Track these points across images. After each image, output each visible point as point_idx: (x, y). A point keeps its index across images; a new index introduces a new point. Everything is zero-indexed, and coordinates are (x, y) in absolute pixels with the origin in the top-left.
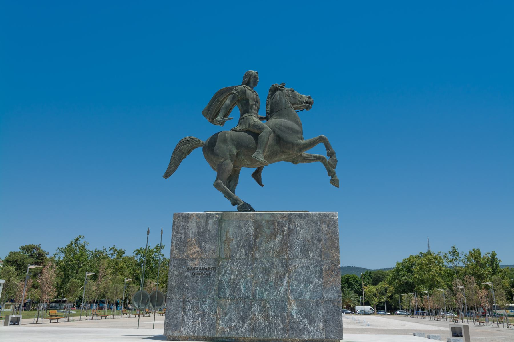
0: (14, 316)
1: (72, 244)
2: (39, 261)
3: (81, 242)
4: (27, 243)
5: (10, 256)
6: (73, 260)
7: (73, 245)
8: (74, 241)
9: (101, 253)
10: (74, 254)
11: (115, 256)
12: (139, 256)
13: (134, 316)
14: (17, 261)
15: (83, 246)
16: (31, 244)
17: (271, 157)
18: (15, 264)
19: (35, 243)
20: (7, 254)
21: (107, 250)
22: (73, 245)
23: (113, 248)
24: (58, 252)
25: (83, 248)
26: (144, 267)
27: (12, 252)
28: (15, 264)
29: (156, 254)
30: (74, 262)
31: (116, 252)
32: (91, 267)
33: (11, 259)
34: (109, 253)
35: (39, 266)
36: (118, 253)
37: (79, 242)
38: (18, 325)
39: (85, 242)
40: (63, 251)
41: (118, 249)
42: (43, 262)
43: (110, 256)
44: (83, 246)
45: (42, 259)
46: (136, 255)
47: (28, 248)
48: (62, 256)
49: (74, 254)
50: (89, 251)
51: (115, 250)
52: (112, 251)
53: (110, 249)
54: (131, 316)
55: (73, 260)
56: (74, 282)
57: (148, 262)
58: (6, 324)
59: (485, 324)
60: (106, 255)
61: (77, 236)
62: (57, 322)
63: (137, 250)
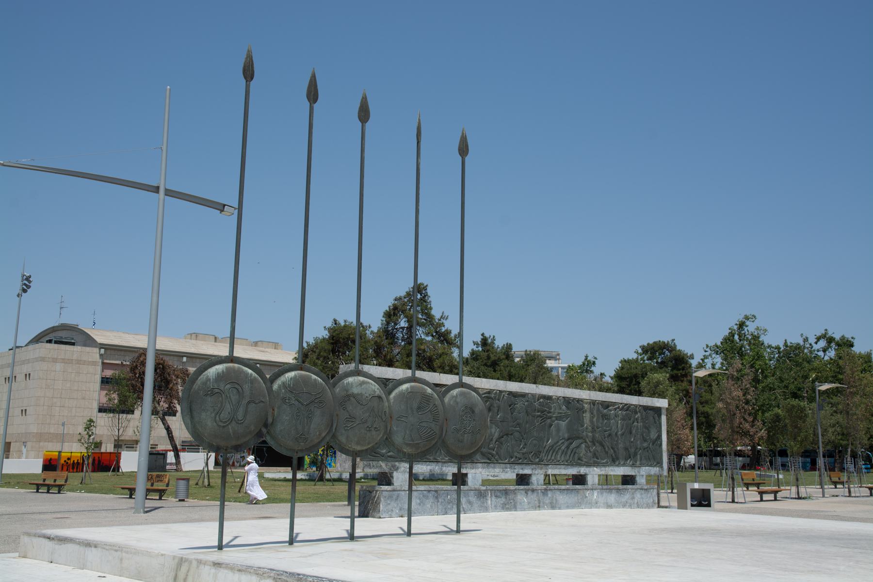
0: (696, 486)
2: (679, 373)
3: (751, 327)
5: (622, 368)
7: (736, 337)
8: (735, 327)
9: (798, 347)
10: (742, 355)
11: (832, 353)
15: (756, 338)
16: (657, 340)
17: (637, 358)
19: (666, 338)
20: (617, 365)
21: (812, 340)
22: (736, 337)
23: (823, 336)
24: (707, 354)
27: (625, 361)
31: (833, 345)
32: (781, 380)
34: (816, 347)
36: (838, 344)
37: (746, 329)
39: (757, 329)
40: (716, 350)
41: (837, 337)
42: (686, 375)
43: (821, 354)
44: (756, 338)
45: (683, 369)
47: (653, 348)
48: (718, 360)
49: (742, 355)
50: (770, 346)
51: (830, 340)
52: (822, 343)
53: (818, 339)
56: (793, 406)
58: (682, 506)
60: (811, 352)
62: (776, 499)
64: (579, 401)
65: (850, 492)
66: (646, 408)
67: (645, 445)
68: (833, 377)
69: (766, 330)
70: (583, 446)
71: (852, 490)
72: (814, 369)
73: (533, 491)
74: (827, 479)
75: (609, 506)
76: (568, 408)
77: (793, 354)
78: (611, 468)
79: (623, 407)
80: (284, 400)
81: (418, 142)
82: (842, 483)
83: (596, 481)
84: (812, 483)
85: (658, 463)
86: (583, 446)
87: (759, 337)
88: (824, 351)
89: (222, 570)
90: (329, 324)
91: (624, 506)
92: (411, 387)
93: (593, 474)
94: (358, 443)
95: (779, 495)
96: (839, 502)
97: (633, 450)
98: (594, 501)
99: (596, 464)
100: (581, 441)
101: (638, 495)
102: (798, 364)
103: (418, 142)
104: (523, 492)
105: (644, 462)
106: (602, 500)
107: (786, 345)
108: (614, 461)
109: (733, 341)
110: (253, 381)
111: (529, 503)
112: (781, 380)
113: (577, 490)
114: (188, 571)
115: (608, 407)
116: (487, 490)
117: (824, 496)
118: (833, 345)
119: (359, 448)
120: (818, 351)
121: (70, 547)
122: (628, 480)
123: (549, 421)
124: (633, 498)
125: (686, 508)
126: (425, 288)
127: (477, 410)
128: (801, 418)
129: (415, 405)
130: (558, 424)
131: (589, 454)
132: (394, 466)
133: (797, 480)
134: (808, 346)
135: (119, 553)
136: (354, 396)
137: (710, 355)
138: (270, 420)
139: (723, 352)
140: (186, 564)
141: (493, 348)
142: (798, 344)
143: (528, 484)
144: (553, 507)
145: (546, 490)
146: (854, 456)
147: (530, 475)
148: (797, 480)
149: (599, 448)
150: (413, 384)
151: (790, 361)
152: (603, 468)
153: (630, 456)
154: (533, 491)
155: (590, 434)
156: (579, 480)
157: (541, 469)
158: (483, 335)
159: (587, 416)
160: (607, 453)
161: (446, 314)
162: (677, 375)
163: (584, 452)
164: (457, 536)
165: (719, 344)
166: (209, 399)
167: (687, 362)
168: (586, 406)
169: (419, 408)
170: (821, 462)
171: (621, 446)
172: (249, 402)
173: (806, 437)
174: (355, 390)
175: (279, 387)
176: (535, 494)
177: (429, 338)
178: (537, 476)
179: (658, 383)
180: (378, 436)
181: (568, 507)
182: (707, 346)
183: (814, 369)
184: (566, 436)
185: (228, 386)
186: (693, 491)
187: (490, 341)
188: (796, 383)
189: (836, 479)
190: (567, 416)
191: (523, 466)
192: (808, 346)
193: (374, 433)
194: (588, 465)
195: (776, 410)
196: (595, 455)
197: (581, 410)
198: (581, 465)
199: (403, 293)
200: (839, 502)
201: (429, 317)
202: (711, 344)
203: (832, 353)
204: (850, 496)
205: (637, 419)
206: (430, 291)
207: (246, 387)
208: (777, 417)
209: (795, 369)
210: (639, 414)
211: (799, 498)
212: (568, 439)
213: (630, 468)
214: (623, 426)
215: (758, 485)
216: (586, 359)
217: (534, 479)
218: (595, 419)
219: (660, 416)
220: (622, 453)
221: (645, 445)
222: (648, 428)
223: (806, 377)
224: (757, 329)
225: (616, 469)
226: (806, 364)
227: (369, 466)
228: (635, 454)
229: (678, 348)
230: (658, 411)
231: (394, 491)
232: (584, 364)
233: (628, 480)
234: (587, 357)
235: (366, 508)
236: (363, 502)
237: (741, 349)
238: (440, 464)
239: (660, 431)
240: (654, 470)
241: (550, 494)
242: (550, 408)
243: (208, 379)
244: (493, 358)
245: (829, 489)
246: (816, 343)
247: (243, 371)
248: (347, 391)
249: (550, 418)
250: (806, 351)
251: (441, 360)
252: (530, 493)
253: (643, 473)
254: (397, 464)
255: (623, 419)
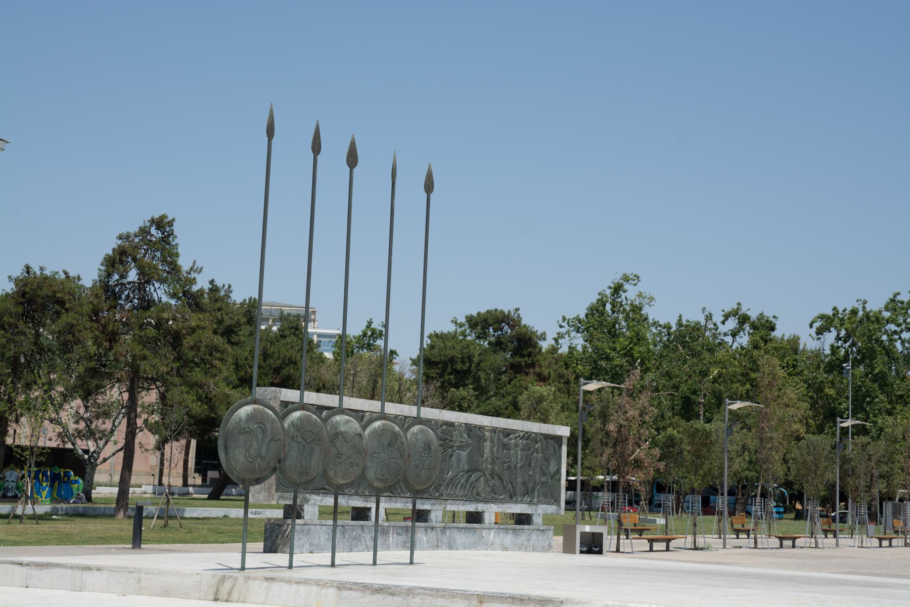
0: (588, 529)
1: (602, 302)
3: (630, 294)
4: (480, 306)
6: (613, 354)
7: (608, 307)
8: (608, 292)
9: (695, 330)
12: (830, 338)
13: (876, 542)
14: (452, 360)
15: (636, 309)
18: (449, 370)
19: (506, 306)
21: (718, 318)
22: (608, 307)
23: (734, 313)
24: (563, 330)
25: (636, 313)
26: (854, 373)
27: (437, 335)
28: (449, 370)
29: (892, 327)
30: (617, 361)
31: (747, 327)
33: (435, 356)
34: (722, 329)
35: (748, 404)
36: (754, 327)
37: (624, 295)
38: (600, 552)
39: (640, 295)
40: (578, 325)
41: (754, 315)
42: (533, 365)
43: (729, 339)
44: (636, 309)
45: (529, 355)
46: (820, 332)
47: (485, 321)
48: (579, 341)
50: (656, 324)
51: (744, 319)
52: (732, 324)
53: (727, 317)
54: (867, 542)
55: (613, 354)
56: (697, 430)
57: (866, 356)
58: (568, 548)
59: (894, 542)
60: (715, 336)
61: (618, 278)
62: (668, 550)
63: (822, 317)
64: (481, 428)
65: (756, 542)
66: (547, 437)
67: (544, 479)
68: (742, 375)
69: (652, 299)
70: (482, 479)
71: (759, 540)
72: (717, 363)
73: (432, 528)
74: (728, 526)
75: (505, 548)
76: (469, 437)
77: (688, 337)
78: (508, 505)
79: (524, 435)
80: (293, 438)
81: (393, 184)
82: (747, 532)
83: (493, 519)
84: (709, 532)
85: (556, 501)
86: (482, 479)
87: (640, 309)
88: (734, 334)
89: (276, 583)
90: (18, 271)
91: (520, 549)
92: (383, 425)
93: (491, 511)
94: (343, 478)
95: (673, 544)
96: (743, 554)
97: (530, 485)
98: (490, 542)
99: (494, 501)
100: (479, 474)
101: (534, 537)
102: (695, 354)
103: (393, 184)
104: (423, 530)
105: (542, 499)
106: (497, 541)
107: (680, 324)
108: (512, 497)
109: (602, 313)
110: (273, 421)
111: (428, 542)
112: (669, 375)
113: (475, 529)
114: (233, 586)
115: (508, 435)
116: (389, 526)
117: (724, 547)
118: (747, 327)
119: (342, 482)
120: (725, 334)
121: (57, 572)
122: (523, 520)
123: (450, 450)
124: (529, 540)
125: (574, 553)
126: (170, 224)
127: (433, 448)
128: (705, 445)
129: (386, 442)
130: (459, 454)
131: (488, 489)
132: (305, 498)
133: (695, 525)
134: (712, 326)
135: (135, 574)
136: (341, 433)
137: (568, 332)
138: (282, 456)
139: (587, 329)
140: (230, 580)
141: (227, 304)
142: (698, 323)
143: (426, 521)
144: (450, 547)
145: (444, 528)
146: (764, 495)
147: (429, 511)
148: (695, 525)
149: (497, 482)
150: (383, 421)
151: (684, 348)
152: (500, 505)
153: (528, 492)
154: (432, 528)
155: (489, 466)
156: (475, 518)
157: (440, 504)
158: (212, 282)
159: (487, 445)
160: (505, 487)
161: (199, 264)
162: (519, 364)
163: (483, 486)
164: (411, 566)
165: (582, 316)
166: (242, 437)
167: (535, 346)
168: (487, 434)
169: (389, 445)
170: (722, 502)
171: (519, 480)
172: (271, 440)
173: (710, 470)
174: (343, 429)
175: (289, 426)
176: (434, 532)
177: (173, 302)
178: (437, 511)
179: (540, 400)
180: (357, 471)
181: (465, 548)
182: (564, 319)
183: (717, 363)
184: (466, 468)
185: (255, 426)
186: (583, 534)
187: (222, 293)
188: (690, 382)
189: (739, 527)
190: (468, 446)
191: (424, 501)
192: (712, 326)
193: (355, 468)
194: (486, 501)
195: (670, 431)
196: (493, 491)
197: (482, 439)
198: (478, 501)
199: (134, 229)
200: (743, 554)
201: (175, 269)
202: (570, 316)
203: (744, 340)
204: (756, 547)
205: (537, 450)
206: (176, 228)
207: (268, 426)
208: (672, 440)
209: (691, 361)
210: (539, 444)
211: (696, 549)
212: (468, 471)
213: (526, 506)
214: (522, 457)
215: (640, 532)
216: (368, 327)
217: (433, 516)
218: (495, 449)
219: (560, 446)
220: (520, 488)
221: (544, 479)
222: (547, 460)
223: (704, 374)
224: (640, 295)
225: (513, 506)
226: (706, 355)
227: (283, 498)
228: (533, 490)
229: (523, 322)
230: (558, 439)
231: (305, 524)
232: (365, 334)
233: (523, 520)
234: (370, 323)
235: (274, 543)
236: (270, 536)
237: (614, 326)
238: (346, 497)
239: (559, 464)
240: (551, 509)
241: (448, 532)
242: (452, 436)
243: (241, 420)
244: (227, 322)
245: (731, 538)
246: (723, 323)
247: (266, 413)
248: (336, 429)
249: (452, 447)
250: (707, 334)
251: (195, 336)
252: (429, 530)
253: (540, 511)
254: (308, 496)
255: (523, 450)
